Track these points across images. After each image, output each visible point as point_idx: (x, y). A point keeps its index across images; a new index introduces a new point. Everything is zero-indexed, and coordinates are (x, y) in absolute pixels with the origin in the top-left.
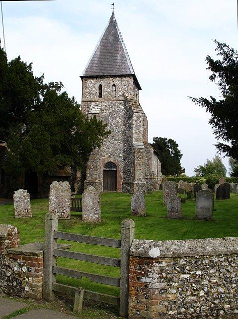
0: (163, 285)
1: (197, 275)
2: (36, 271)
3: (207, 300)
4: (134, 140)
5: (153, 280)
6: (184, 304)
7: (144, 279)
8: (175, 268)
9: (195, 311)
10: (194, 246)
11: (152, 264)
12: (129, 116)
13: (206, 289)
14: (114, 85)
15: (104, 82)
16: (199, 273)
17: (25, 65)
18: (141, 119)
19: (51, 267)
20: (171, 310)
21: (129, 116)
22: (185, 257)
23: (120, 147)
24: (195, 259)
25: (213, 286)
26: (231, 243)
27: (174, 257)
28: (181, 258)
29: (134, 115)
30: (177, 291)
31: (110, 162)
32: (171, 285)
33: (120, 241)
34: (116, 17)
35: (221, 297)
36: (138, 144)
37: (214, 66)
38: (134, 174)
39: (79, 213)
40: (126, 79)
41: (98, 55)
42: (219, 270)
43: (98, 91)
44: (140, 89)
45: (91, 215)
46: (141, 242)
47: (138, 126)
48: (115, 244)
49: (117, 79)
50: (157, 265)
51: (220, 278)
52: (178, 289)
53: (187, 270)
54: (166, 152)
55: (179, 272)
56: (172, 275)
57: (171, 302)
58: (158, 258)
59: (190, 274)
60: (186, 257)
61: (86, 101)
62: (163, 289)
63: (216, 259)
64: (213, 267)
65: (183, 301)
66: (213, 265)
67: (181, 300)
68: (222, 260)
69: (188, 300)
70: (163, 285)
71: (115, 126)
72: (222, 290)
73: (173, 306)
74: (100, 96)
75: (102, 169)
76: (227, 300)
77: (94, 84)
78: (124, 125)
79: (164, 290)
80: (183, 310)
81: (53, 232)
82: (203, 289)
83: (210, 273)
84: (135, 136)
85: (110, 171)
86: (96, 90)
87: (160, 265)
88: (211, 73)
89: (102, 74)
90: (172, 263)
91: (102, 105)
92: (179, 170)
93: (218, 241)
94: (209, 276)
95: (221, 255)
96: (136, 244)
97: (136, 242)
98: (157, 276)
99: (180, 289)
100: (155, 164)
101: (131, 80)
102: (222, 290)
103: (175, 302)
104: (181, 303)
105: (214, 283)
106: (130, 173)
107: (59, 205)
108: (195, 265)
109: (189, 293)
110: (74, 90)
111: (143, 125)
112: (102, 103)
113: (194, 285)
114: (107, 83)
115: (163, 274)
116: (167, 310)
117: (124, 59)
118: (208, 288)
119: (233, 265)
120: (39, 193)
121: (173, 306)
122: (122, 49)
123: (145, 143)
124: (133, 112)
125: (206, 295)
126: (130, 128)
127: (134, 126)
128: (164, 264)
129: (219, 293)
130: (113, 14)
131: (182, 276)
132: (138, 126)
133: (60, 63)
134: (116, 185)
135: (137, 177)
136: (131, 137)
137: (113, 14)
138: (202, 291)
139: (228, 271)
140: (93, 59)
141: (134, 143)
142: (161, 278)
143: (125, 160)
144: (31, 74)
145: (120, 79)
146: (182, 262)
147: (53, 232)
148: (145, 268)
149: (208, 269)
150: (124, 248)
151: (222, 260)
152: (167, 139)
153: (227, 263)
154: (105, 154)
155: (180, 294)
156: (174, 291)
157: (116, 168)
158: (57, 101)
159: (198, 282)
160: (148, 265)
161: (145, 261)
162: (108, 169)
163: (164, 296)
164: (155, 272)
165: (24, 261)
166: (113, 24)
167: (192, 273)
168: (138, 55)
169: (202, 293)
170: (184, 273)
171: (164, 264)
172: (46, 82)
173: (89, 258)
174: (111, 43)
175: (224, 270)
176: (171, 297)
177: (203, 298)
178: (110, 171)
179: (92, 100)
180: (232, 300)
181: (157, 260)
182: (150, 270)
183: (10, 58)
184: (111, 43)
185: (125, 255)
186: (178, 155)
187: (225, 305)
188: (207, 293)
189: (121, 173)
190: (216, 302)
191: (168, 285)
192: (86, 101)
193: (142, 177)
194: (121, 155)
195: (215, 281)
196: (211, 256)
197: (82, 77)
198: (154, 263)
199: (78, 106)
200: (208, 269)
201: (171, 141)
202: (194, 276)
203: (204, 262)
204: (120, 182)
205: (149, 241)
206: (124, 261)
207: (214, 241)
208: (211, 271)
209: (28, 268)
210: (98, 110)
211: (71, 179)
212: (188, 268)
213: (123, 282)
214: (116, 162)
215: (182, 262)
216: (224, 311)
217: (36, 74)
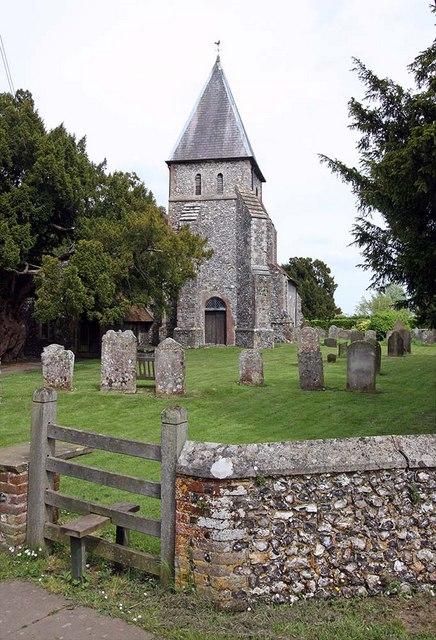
0: (240, 534)
1: (309, 513)
2: (14, 501)
4: (252, 262)
5: (220, 523)
6: (283, 573)
7: (202, 522)
8: (263, 499)
9: (307, 589)
10: (301, 455)
12: (245, 224)
13: (327, 541)
14: (220, 175)
15: (204, 171)
16: (312, 508)
17: (72, 140)
18: (264, 228)
19: (42, 494)
20: (258, 584)
21: (245, 224)
22: (282, 476)
24: (304, 478)
26: (423, 449)
28: (274, 479)
31: (212, 298)
32: (255, 533)
33: (160, 448)
34: (224, 66)
35: (360, 559)
36: (258, 266)
37: (366, 120)
38: (254, 317)
39: (150, 383)
40: (240, 164)
41: (195, 122)
42: (353, 503)
43: (194, 185)
44: (262, 180)
45: (170, 386)
46: (200, 446)
47: (259, 240)
48: (152, 455)
49: (224, 164)
50: (227, 492)
51: (356, 519)
54: (310, 282)
55: (271, 507)
58: (227, 480)
59: (294, 510)
60: (284, 477)
62: (240, 542)
63: (345, 481)
64: (340, 497)
65: (282, 566)
66: (340, 492)
67: (277, 564)
68: (358, 482)
69: (291, 563)
70: (240, 534)
71: (221, 240)
74: (199, 192)
75: (203, 309)
76: (372, 565)
77: (188, 175)
78: (237, 238)
79: (240, 545)
80: (281, 585)
81: (45, 425)
82: (321, 542)
83: (335, 509)
84: (254, 255)
85: (216, 312)
86: (191, 183)
87: (234, 493)
88: (360, 135)
89: (200, 157)
91: (202, 207)
92: (332, 310)
93: (352, 443)
95: (355, 472)
96: (188, 452)
98: (228, 515)
99: (275, 543)
100: (292, 301)
101: (247, 167)
102: (360, 543)
103: (265, 569)
104: (276, 571)
105: (343, 529)
106: (247, 317)
107: (117, 370)
108: (304, 491)
109: (294, 550)
110: (159, 187)
111: (268, 237)
113: (302, 534)
114: (208, 173)
115: (241, 511)
116: (250, 585)
117: (235, 132)
119: (382, 493)
120: (87, 346)
122: (231, 116)
123: (273, 267)
125: (328, 554)
126: (247, 243)
127: (253, 239)
128: (241, 490)
129: (353, 549)
130: (218, 61)
131: (279, 514)
132: (259, 240)
133: (128, 137)
134: (225, 336)
135: (258, 321)
137: (218, 61)
138: (319, 546)
139: (371, 504)
140: (186, 134)
141: (253, 265)
142: (236, 519)
144: (84, 157)
145: (229, 165)
147: (45, 425)
150: (167, 462)
151: (358, 482)
152: (311, 260)
153: (368, 489)
156: (262, 545)
157: (225, 306)
158: (125, 194)
159: (310, 528)
160: (210, 492)
161: (203, 484)
162: (212, 309)
164: (223, 508)
166: (217, 73)
167: (297, 508)
168: (259, 127)
169: (319, 550)
170: (284, 509)
171: (241, 490)
172: (108, 171)
173: (109, 479)
174: (215, 105)
175: (363, 504)
176: (256, 558)
177: (322, 560)
178: (216, 312)
180: (383, 565)
181: (228, 482)
182: (214, 503)
183: (49, 126)
184: (215, 105)
185: (168, 477)
186: (330, 286)
187: (369, 576)
189: (233, 316)
190: (350, 568)
191: (250, 534)
193: (266, 321)
194: (232, 286)
195: (345, 525)
196: (335, 474)
197: (169, 163)
199: (161, 212)
201: (319, 264)
202: (303, 515)
203: (322, 487)
204: (233, 329)
205: (215, 445)
206: (167, 488)
207: (342, 444)
208: (338, 505)
210: (194, 215)
211: (139, 326)
213: (166, 528)
214: (224, 297)
215: (278, 486)
216: (367, 587)
217: (94, 156)
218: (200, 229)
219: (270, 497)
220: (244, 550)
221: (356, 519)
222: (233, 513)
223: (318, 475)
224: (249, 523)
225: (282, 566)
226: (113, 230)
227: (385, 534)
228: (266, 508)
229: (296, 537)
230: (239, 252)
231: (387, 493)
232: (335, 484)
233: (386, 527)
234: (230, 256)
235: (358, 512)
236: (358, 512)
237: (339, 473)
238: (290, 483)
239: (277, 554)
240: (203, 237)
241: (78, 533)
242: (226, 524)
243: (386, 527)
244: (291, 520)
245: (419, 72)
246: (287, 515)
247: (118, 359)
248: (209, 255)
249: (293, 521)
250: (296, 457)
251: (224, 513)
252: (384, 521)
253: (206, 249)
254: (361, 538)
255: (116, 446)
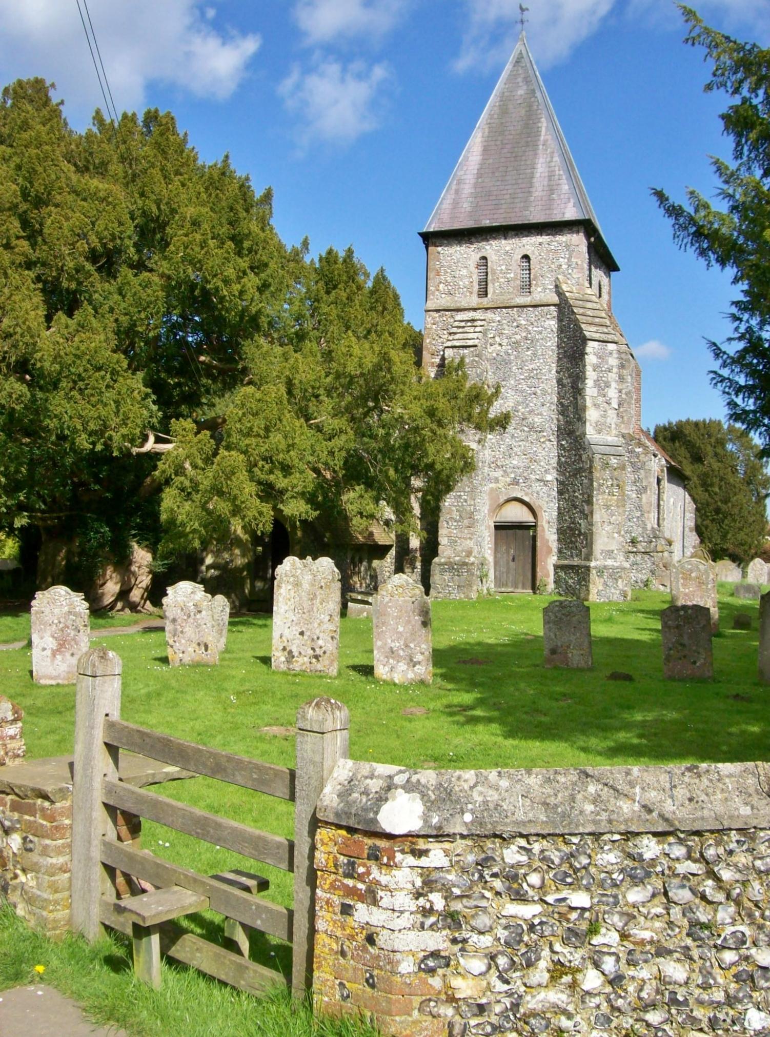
0: (437, 940)
3: (614, 1008)
7: (362, 913)
8: (482, 877)
11: (391, 857)
13: (609, 964)
14: (526, 257)
15: (494, 249)
16: (580, 899)
18: (613, 361)
22: (521, 836)
23: (547, 454)
25: (638, 956)
26: (727, 788)
27: (487, 835)
28: (505, 840)
29: (588, 350)
30: (489, 968)
32: (465, 941)
35: (674, 1001)
42: (666, 894)
43: (475, 279)
47: (603, 386)
50: (410, 860)
51: (670, 924)
52: (493, 958)
53: (531, 886)
55: (498, 894)
56: (472, 903)
57: (464, 1008)
61: (437, 311)
62: (435, 954)
63: (650, 848)
64: (636, 881)
65: (515, 1006)
67: (507, 1002)
69: (532, 1003)
70: (437, 940)
72: (676, 971)
73: (473, 1022)
74: (484, 293)
79: (433, 962)
81: (100, 721)
82: (597, 965)
83: (627, 904)
86: (468, 274)
87: (424, 862)
90: (471, 858)
94: (622, 914)
97: (343, 769)
98: (412, 905)
99: (502, 961)
101: (579, 241)
102: (676, 971)
104: (503, 1014)
105: (642, 943)
108: (565, 867)
109: (540, 974)
112: (489, 315)
113: (557, 947)
118: (618, 960)
121: (473, 1022)
124: (585, 340)
125: (608, 989)
128: (437, 857)
136: (581, 420)
141: (591, 433)
143: (560, 493)
146: (512, 855)
148: (368, 873)
149: (615, 885)
154: (499, 473)
155: (500, 977)
156: (477, 965)
163: (436, 982)
165: (16, 816)
167: (550, 899)
169: (592, 980)
170: (520, 897)
175: (684, 895)
177: (597, 1000)
179: (458, 305)
181: (412, 843)
182: (384, 879)
188: (616, 981)
189: (549, 536)
191: (454, 941)
192: (437, 311)
194: (549, 477)
195: (647, 935)
196: (629, 835)
198: (399, 857)
200: (615, 885)
202: (562, 911)
204: (549, 562)
209: (25, 839)
212: (534, 879)
215: (512, 855)
218: (486, 365)
219: (495, 875)
220: (440, 971)
221: (670, 924)
222: (422, 901)
223: (596, 836)
224: (452, 920)
225: (515, 1006)
226: (307, 368)
227: (729, 956)
228: (488, 894)
229: (546, 953)
230: (563, 410)
231: (738, 876)
232: (630, 856)
233: (731, 943)
234: (545, 415)
235: (676, 912)
236: (676, 912)
237: (638, 834)
238: (536, 847)
239: (507, 982)
240: (491, 379)
241: (144, 918)
242: (406, 921)
243: (731, 943)
244: (536, 921)
245: (177, 213)
246: (529, 911)
247: (305, 612)
248: (502, 422)
249: (541, 923)
250: (552, 801)
251: (404, 900)
252: (730, 929)
253: (495, 411)
254: (678, 960)
255: (219, 768)
